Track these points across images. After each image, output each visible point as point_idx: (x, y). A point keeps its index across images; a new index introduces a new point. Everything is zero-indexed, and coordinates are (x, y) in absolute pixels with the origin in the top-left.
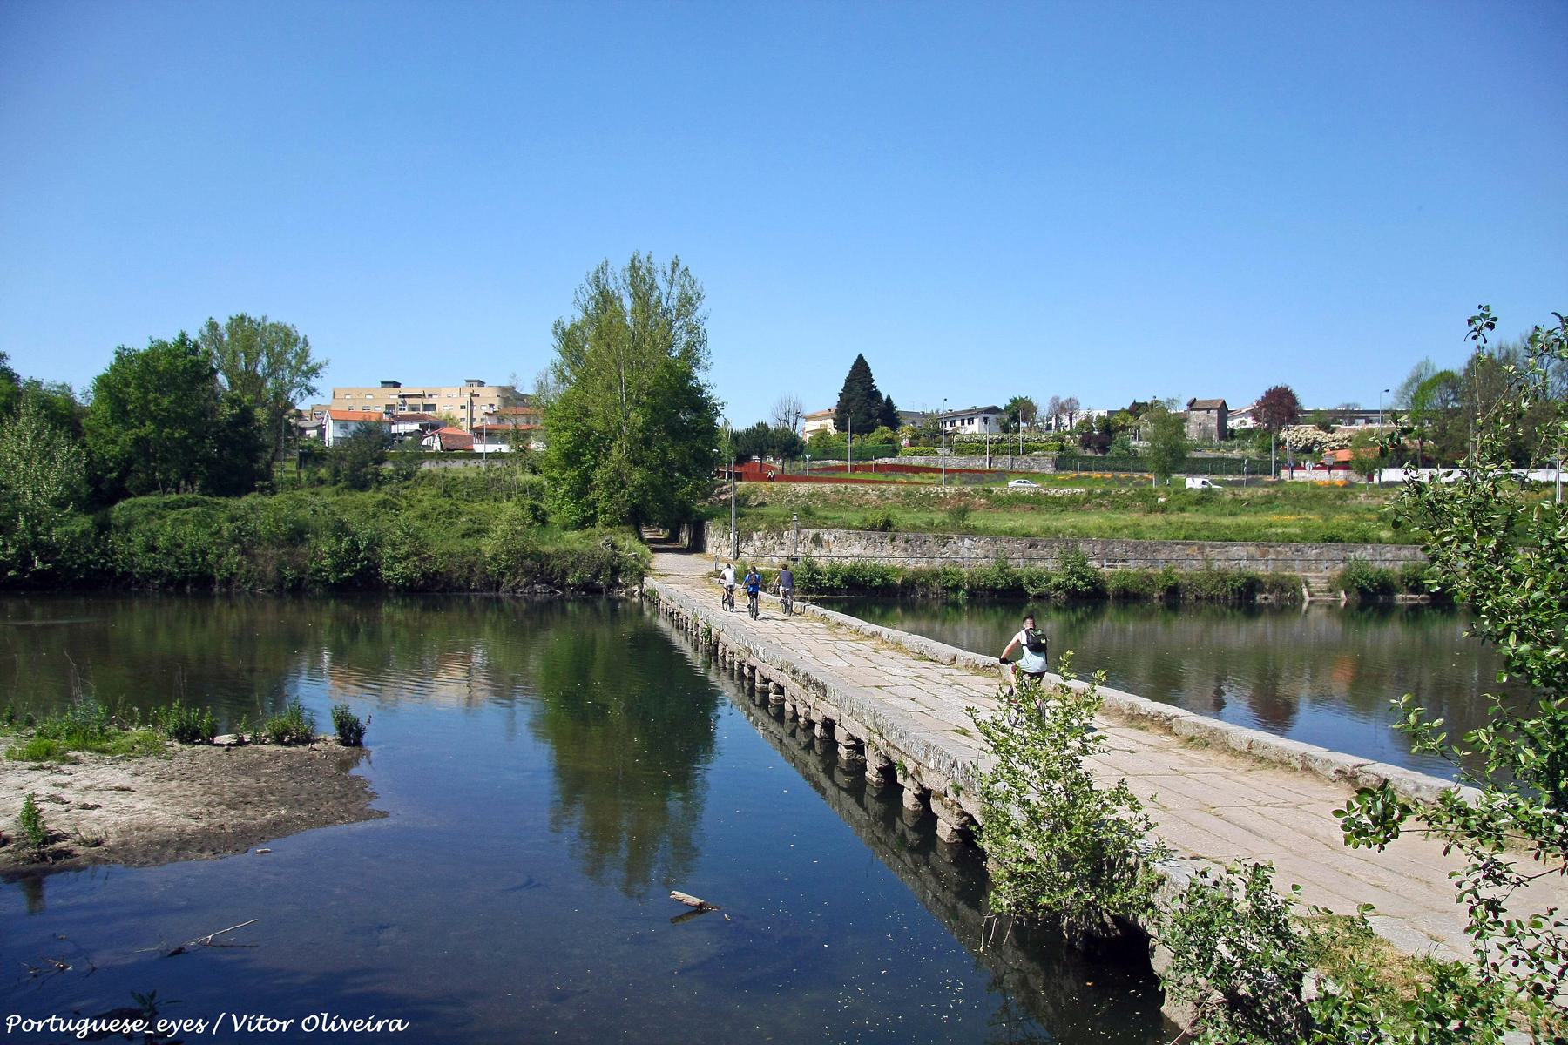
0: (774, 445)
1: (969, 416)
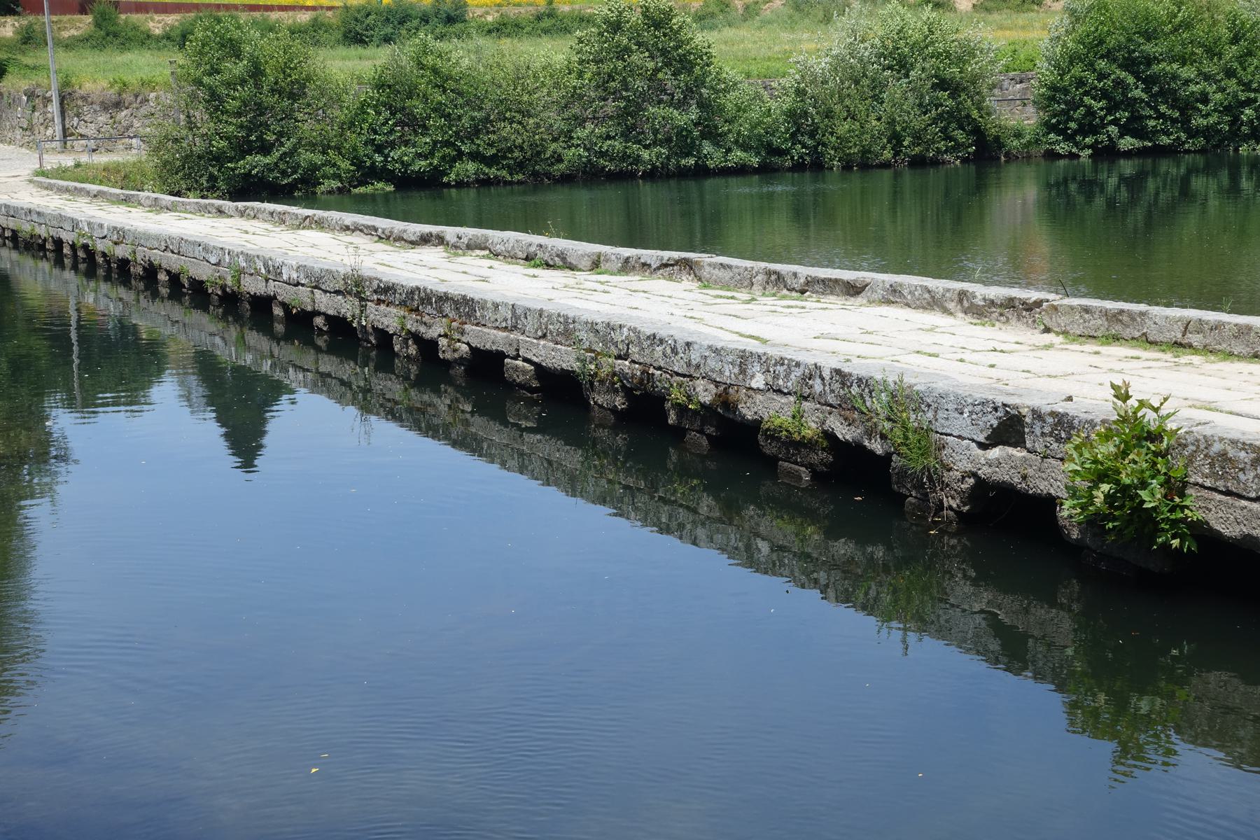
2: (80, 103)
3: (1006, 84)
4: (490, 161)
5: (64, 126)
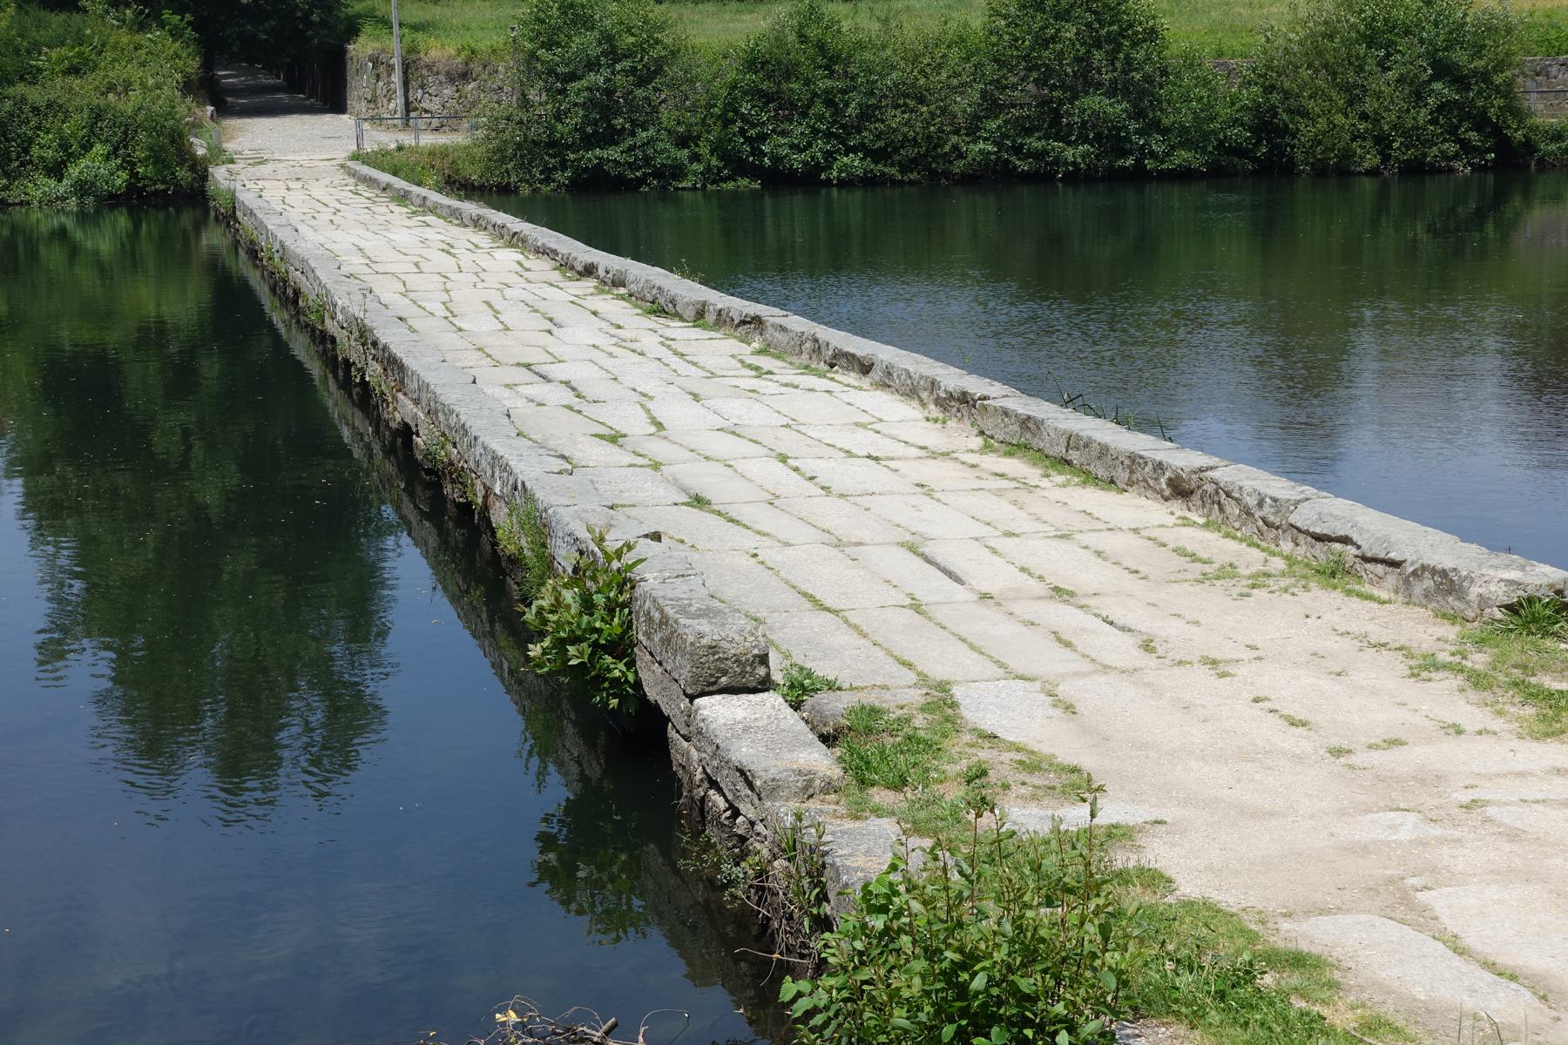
2: (425, 72)
3: (1554, 70)
5: (407, 99)
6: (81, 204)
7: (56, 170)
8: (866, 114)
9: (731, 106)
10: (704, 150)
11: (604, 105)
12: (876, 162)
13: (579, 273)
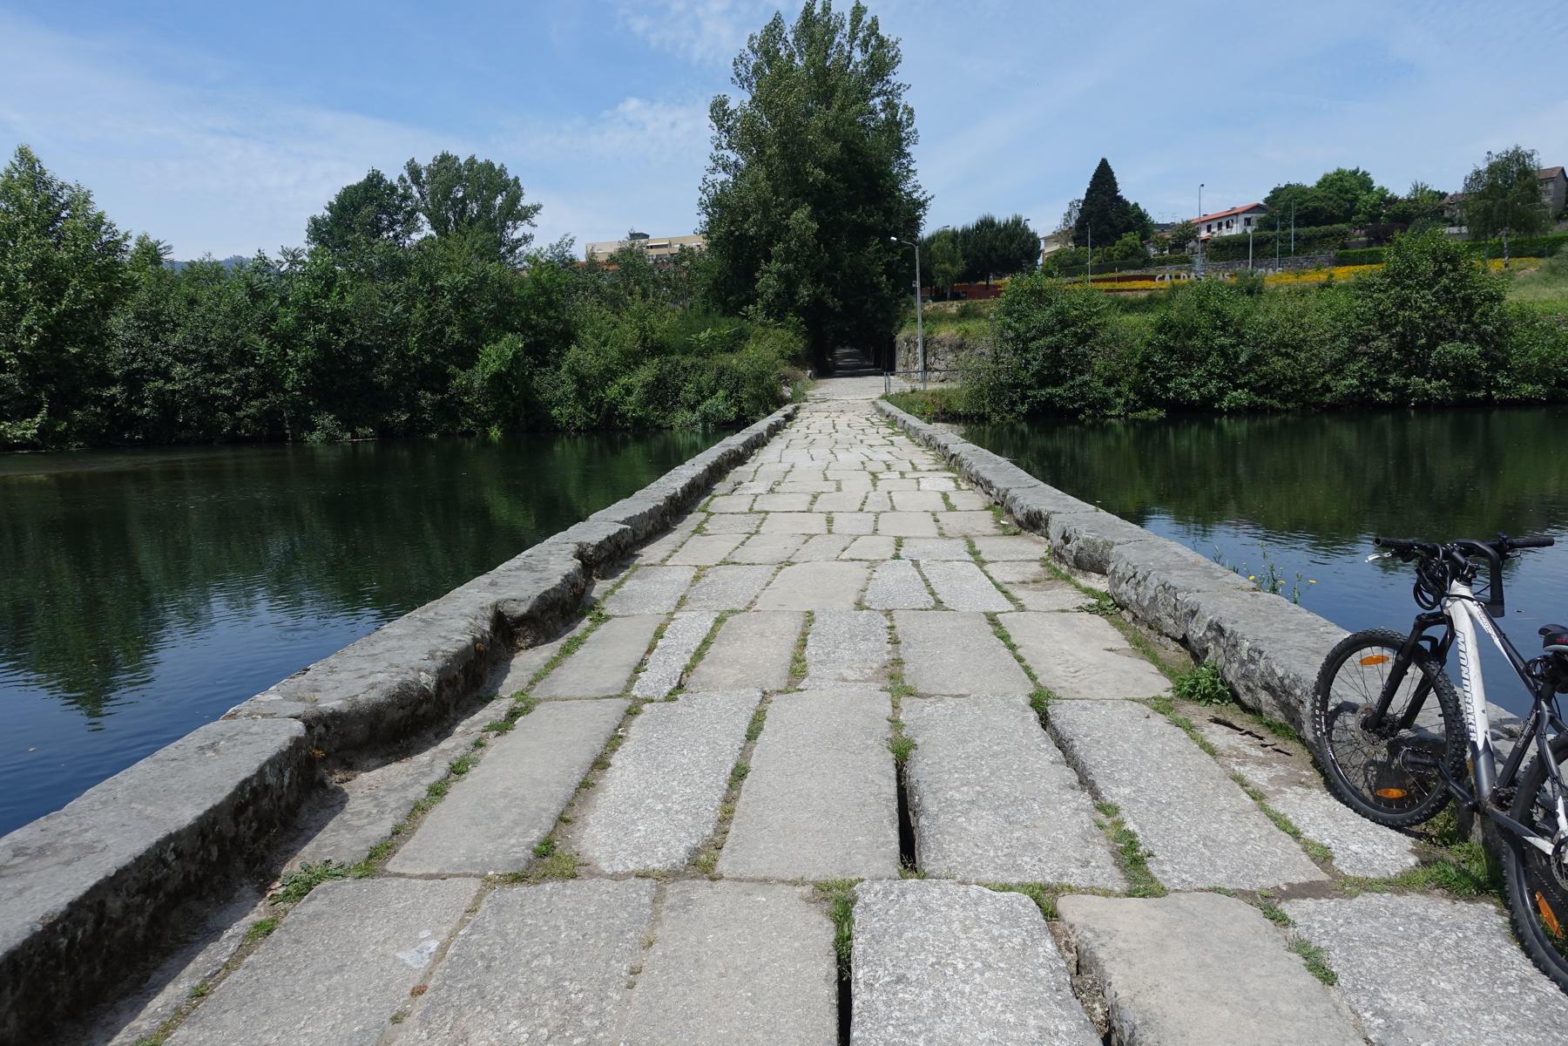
0: (996, 250)
1: (1227, 219)
4: (1260, 391)
6: (705, 428)
7: (692, 408)
8: (1255, 360)
9: (1147, 358)
10: (1125, 389)
11: (1054, 356)
12: (1259, 395)
13: (1019, 523)
